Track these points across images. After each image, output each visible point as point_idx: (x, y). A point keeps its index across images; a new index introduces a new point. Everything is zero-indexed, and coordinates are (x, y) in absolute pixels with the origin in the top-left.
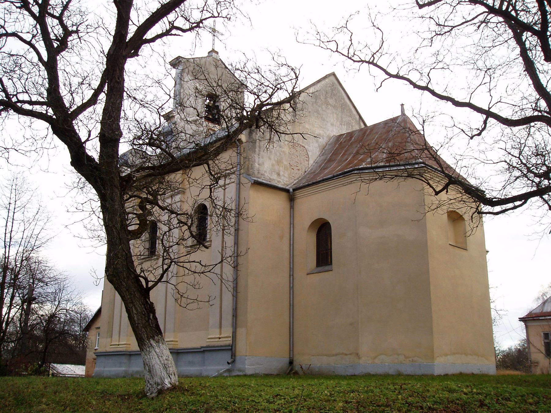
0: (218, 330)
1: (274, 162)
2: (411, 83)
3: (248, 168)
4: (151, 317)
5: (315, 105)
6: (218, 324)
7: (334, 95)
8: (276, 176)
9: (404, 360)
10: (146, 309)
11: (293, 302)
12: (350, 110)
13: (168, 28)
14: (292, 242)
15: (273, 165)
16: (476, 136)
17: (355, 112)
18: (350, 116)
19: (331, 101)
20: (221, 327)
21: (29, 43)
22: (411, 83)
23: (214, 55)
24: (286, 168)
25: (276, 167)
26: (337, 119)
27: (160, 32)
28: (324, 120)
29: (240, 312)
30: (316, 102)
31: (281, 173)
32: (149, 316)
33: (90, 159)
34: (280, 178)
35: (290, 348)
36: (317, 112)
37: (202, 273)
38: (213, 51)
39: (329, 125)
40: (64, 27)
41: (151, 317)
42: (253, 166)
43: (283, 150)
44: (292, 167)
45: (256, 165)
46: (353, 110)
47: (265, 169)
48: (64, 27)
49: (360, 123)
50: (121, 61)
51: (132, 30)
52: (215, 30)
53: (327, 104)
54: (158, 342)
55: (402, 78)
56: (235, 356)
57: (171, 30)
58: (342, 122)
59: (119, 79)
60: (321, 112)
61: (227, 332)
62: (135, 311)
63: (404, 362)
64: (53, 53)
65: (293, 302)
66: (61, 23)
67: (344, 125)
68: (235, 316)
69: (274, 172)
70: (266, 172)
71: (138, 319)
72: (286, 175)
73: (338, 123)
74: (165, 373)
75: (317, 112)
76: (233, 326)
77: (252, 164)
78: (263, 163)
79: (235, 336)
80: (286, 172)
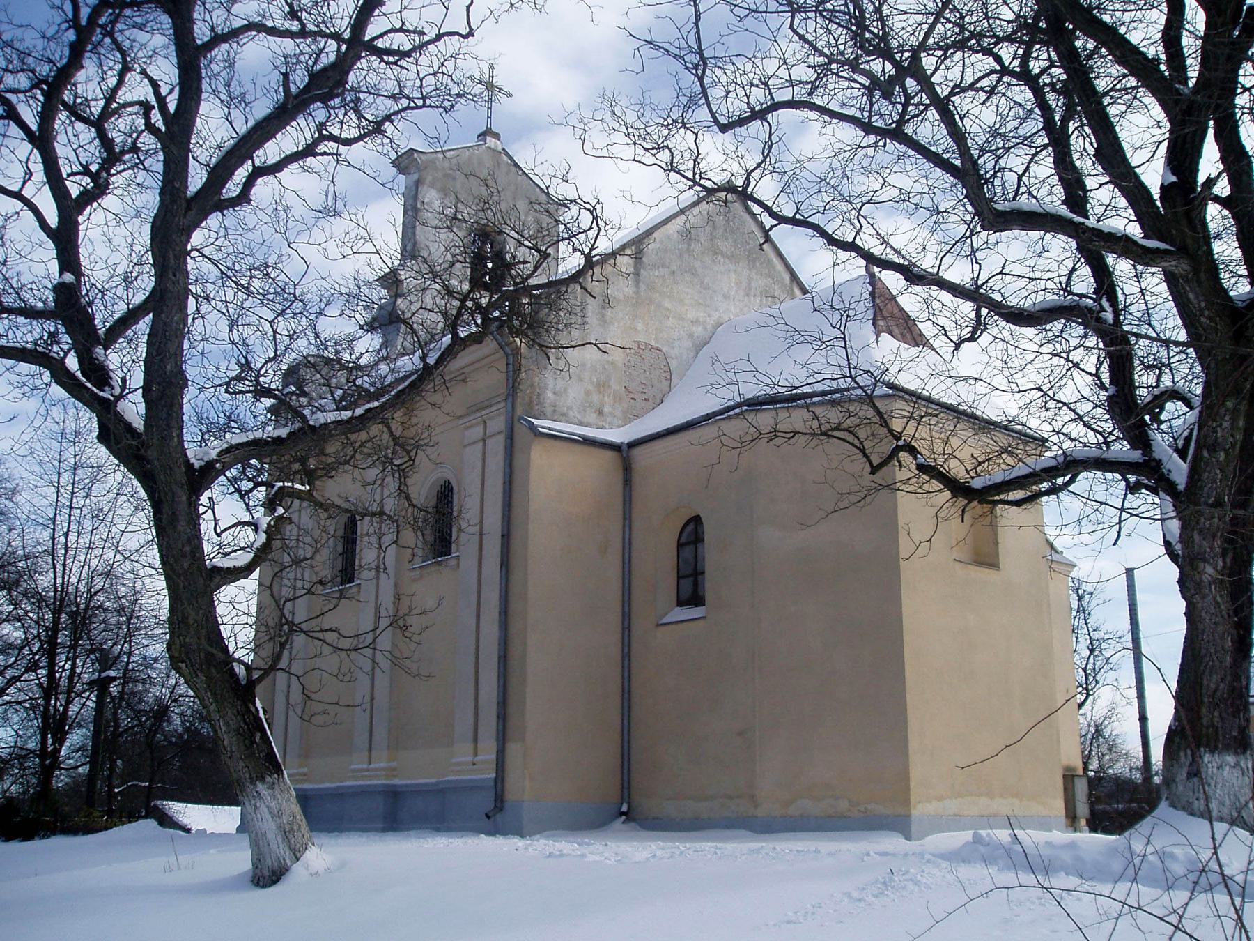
0: (470, 746)
1: (590, 387)
2: (823, 234)
3: (531, 402)
4: (257, 739)
5: (686, 256)
6: (471, 734)
7: (732, 232)
8: (594, 415)
9: (849, 810)
10: (246, 723)
11: (629, 685)
12: (769, 261)
13: (310, 140)
14: (627, 555)
15: (588, 393)
16: (966, 343)
17: (779, 267)
18: (769, 275)
19: (724, 245)
20: (476, 740)
21: (18, 195)
22: (823, 234)
23: (491, 141)
24: (617, 398)
25: (595, 398)
26: (738, 283)
27: (291, 149)
28: (707, 288)
29: (512, 710)
30: (688, 249)
31: (607, 409)
32: (253, 735)
33: (129, 427)
34: (605, 421)
35: (622, 784)
36: (693, 273)
37: (356, 650)
38: (487, 133)
39: (720, 298)
40: (106, 142)
41: (257, 739)
42: (541, 397)
43: (610, 359)
44: (632, 396)
45: (549, 394)
46: (776, 261)
47: (569, 403)
48: (106, 142)
49: (792, 290)
50: (178, 240)
51: (196, 179)
52: (493, 86)
53: (716, 252)
54: (272, 786)
55: (804, 223)
56: (502, 801)
57: (316, 142)
58: (750, 289)
59: (174, 275)
60: (700, 271)
61: (488, 753)
62: (223, 729)
63: (849, 814)
64: (70, 208)
65: (629, 685)
66: (102, 136)
67: (755, 296)
68: (502, 717)
69: (590, 406)
70: (570, 408)
71: (231, 744)
72: (618, 413)
73: (741, 293)
74: (286, 849)
75: (693, 273)
76: (497, 740)
77: (539, 395)
78: (565, 390)
79: (503, 762)
80: (617, 405)
